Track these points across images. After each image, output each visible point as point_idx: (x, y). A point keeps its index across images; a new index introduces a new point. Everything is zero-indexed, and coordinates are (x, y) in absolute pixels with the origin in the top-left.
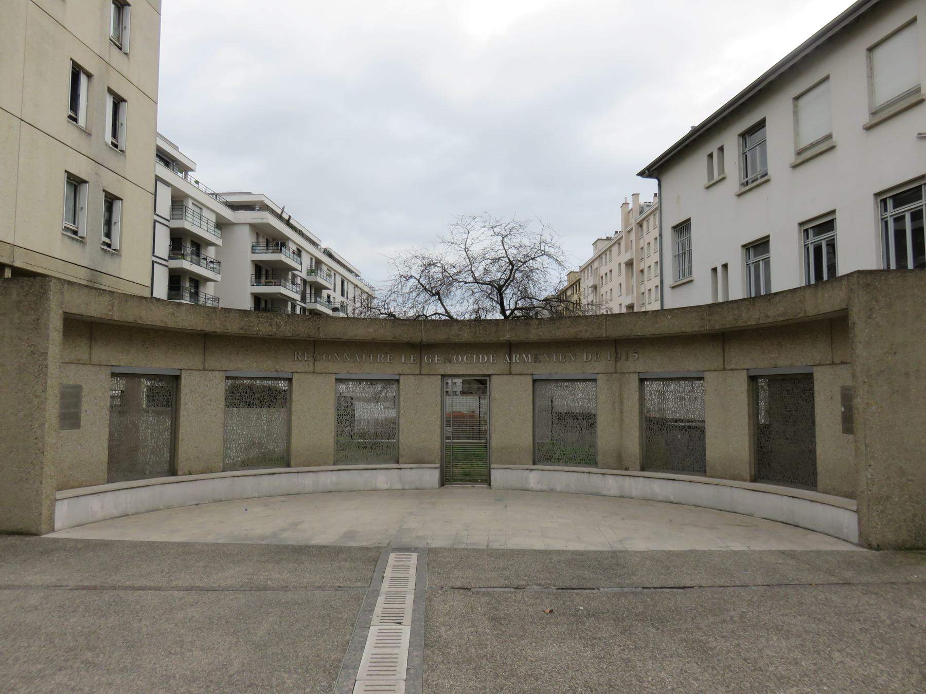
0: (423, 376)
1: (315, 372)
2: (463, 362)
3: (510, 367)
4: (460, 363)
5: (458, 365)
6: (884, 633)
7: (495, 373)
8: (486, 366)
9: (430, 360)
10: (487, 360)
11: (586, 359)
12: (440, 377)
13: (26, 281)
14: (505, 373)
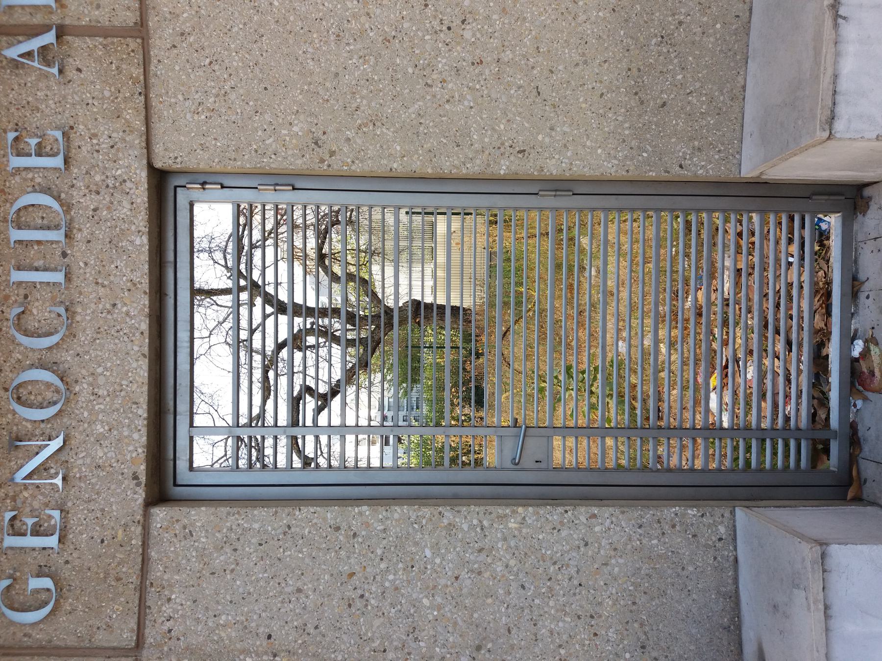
0: (151, 635)
1: (130, 18)
2: (67, 358)
3: (91, 31)
4: (67, 207)
5: (83, 388)
6: (439, 97)
7: (138, 141)
8: (90, 201)
9: (36, 583)
10: (47, 190)
11: (57, 227)
12: (160, 514)
13: (799, 431)
14: (137, 72)
